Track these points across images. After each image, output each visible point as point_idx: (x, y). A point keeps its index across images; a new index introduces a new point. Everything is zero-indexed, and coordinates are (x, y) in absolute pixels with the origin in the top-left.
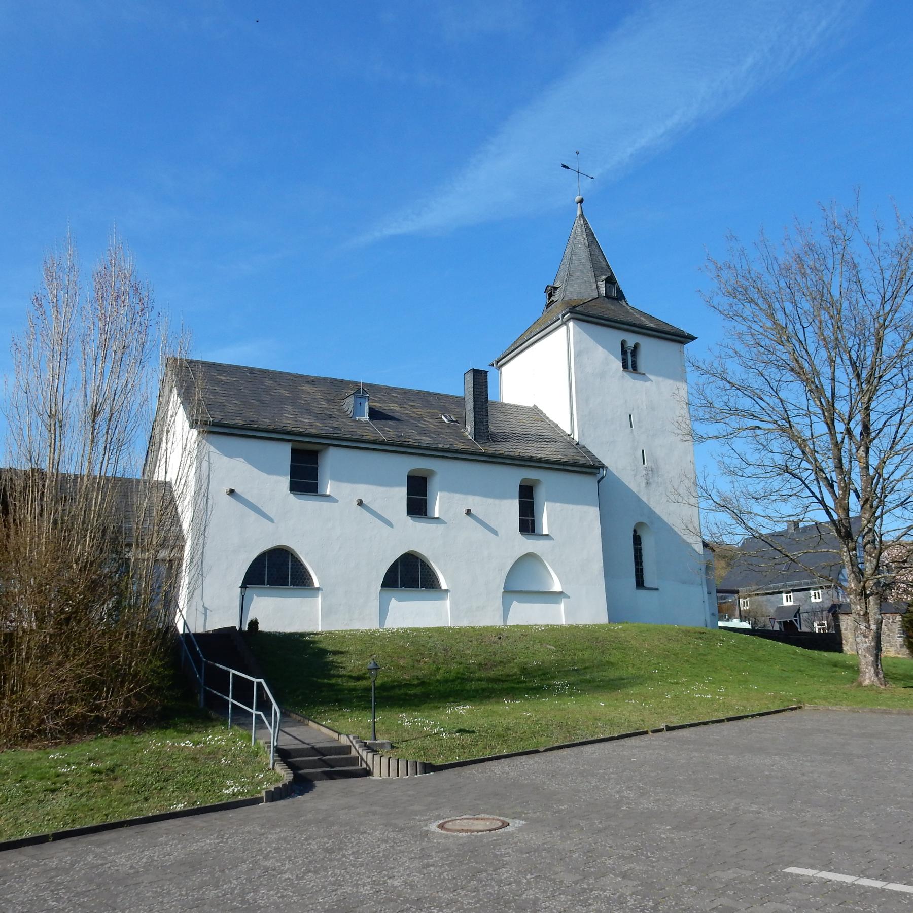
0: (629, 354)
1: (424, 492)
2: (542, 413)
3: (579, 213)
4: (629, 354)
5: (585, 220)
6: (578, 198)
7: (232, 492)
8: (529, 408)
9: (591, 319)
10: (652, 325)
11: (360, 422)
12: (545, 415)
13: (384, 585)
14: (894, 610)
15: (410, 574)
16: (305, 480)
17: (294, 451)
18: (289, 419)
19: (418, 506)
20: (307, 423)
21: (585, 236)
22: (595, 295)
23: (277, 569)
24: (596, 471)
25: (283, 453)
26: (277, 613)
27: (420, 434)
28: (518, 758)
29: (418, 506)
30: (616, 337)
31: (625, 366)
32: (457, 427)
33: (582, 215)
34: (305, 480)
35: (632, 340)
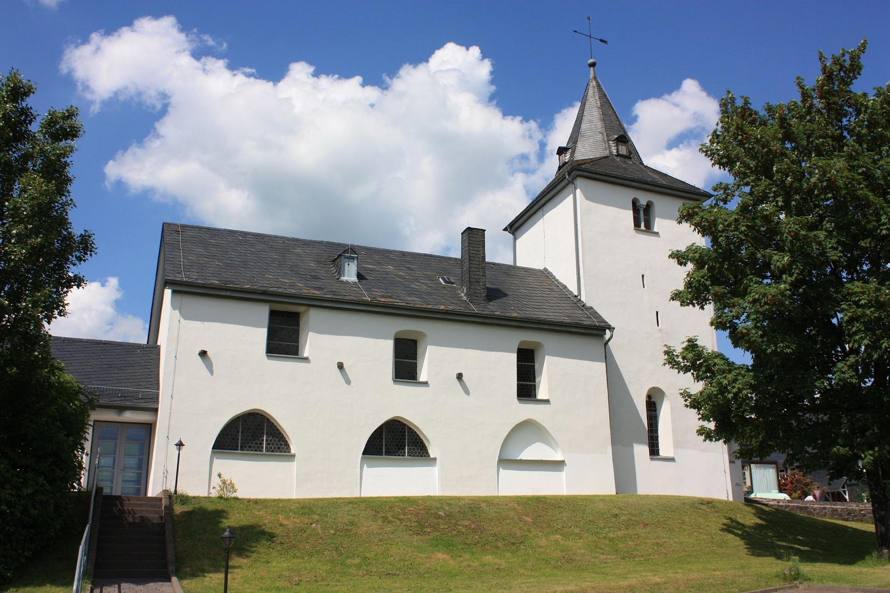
0: (642, 213)
1: (414, 356)
2: (552, 275)
3: (592, 76)
4: (642, 213)
5: (597, 82)
6: (591, 61)
7: (203, 354)
8: (539, 271)
9: (597, 176)
10: (664, 182)
11: (347, 282)
12: (554, 278)
13: (364, 453)
14: (167, 239)
15: (395, 441)
16: (284, 341)
17: (273, 314)
18: (271, 280)
19: (406, 367)
20: (288, 283)
21: (597, 98)
22: (607, 153)
23: (250, 434)
24: (600, 333)
25: (263, 312)
26: (254, 479)
27: (410, 295)
28: (229, 582)
29: (406, 367)
30: (629, 195)
31: (637, 225)
32: (455, 288)
33: (595, 78)
34: (284, 341)
35: (644, 199)
